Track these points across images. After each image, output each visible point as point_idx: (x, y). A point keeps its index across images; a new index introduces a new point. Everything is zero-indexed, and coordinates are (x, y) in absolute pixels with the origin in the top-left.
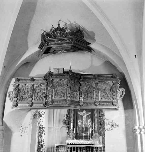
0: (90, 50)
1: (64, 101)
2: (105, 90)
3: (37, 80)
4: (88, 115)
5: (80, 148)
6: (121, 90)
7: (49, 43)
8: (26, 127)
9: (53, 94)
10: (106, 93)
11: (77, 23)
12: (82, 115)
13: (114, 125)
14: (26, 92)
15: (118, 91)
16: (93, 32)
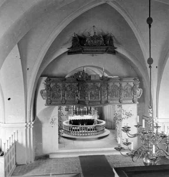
0: (114, 52)
2: (127, 89)
6: (139, 90)
8: (55, 119)
14: (57, 90)
15: (137, 90)
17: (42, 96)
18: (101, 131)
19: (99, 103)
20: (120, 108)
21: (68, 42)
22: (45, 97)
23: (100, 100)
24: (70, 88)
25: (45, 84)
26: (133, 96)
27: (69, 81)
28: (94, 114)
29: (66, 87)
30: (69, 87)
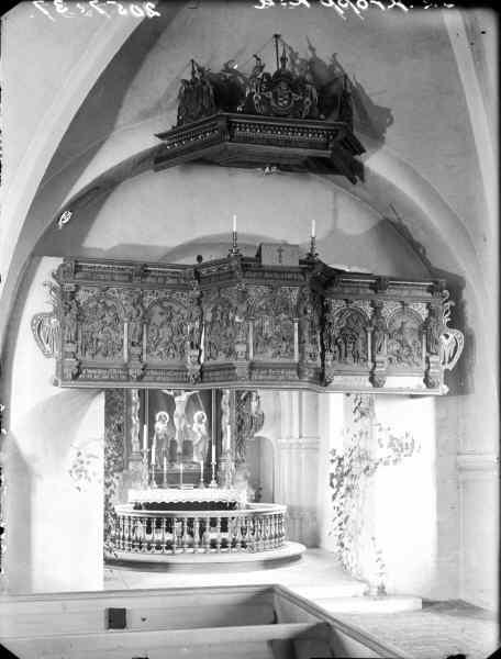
1: (292, 369)
2: (401, 331)
3: (157, 277)
4: (195, 394)
5: (202, 521)
6: (451, 336)
7: (237, 131)
9: (251, 342)
10: (403, 343)
11: (340, 61)
12: (172, 393)
13: (402, 448)
14: (108, 319)
15: (443, 337)
16: (388, 110)
17: (38, 339)
18: (271, 538)
19: (295, 372)
20: (366, 421)
21: (158, 108)
22: (52, 346)
23: (296, 359)
24: (162, 314)
25: (54, 289)
26: (427, 358)
27: (160, 280)
28: (233, 483)
29: (147, 305)
30: (158, 309)
